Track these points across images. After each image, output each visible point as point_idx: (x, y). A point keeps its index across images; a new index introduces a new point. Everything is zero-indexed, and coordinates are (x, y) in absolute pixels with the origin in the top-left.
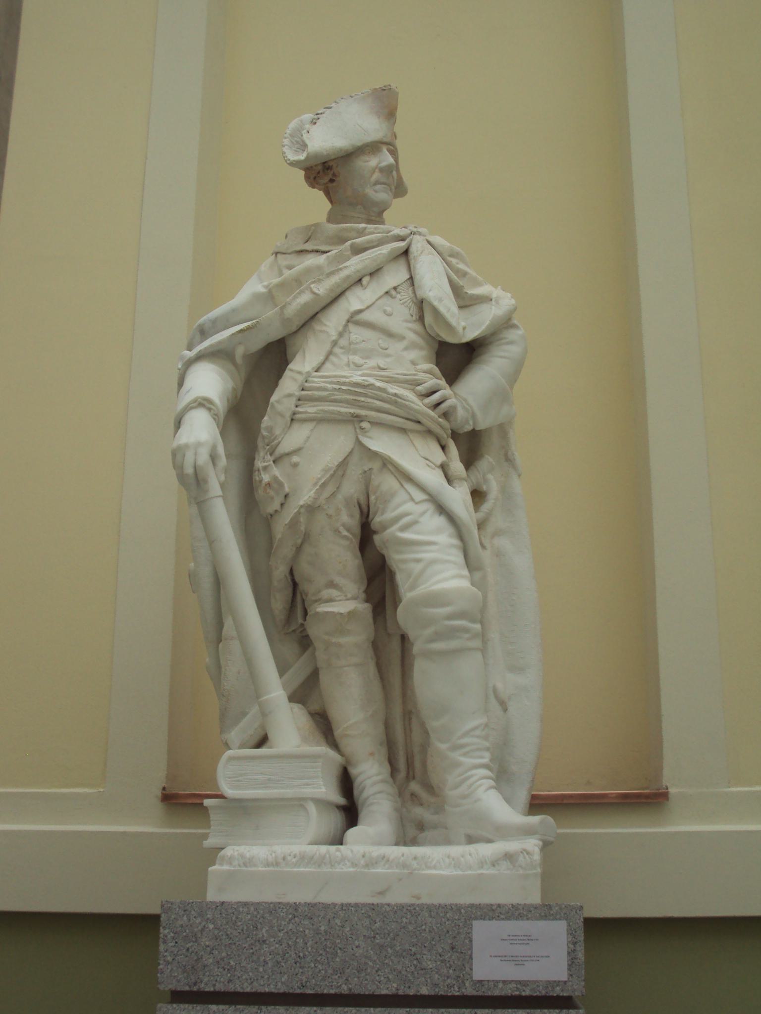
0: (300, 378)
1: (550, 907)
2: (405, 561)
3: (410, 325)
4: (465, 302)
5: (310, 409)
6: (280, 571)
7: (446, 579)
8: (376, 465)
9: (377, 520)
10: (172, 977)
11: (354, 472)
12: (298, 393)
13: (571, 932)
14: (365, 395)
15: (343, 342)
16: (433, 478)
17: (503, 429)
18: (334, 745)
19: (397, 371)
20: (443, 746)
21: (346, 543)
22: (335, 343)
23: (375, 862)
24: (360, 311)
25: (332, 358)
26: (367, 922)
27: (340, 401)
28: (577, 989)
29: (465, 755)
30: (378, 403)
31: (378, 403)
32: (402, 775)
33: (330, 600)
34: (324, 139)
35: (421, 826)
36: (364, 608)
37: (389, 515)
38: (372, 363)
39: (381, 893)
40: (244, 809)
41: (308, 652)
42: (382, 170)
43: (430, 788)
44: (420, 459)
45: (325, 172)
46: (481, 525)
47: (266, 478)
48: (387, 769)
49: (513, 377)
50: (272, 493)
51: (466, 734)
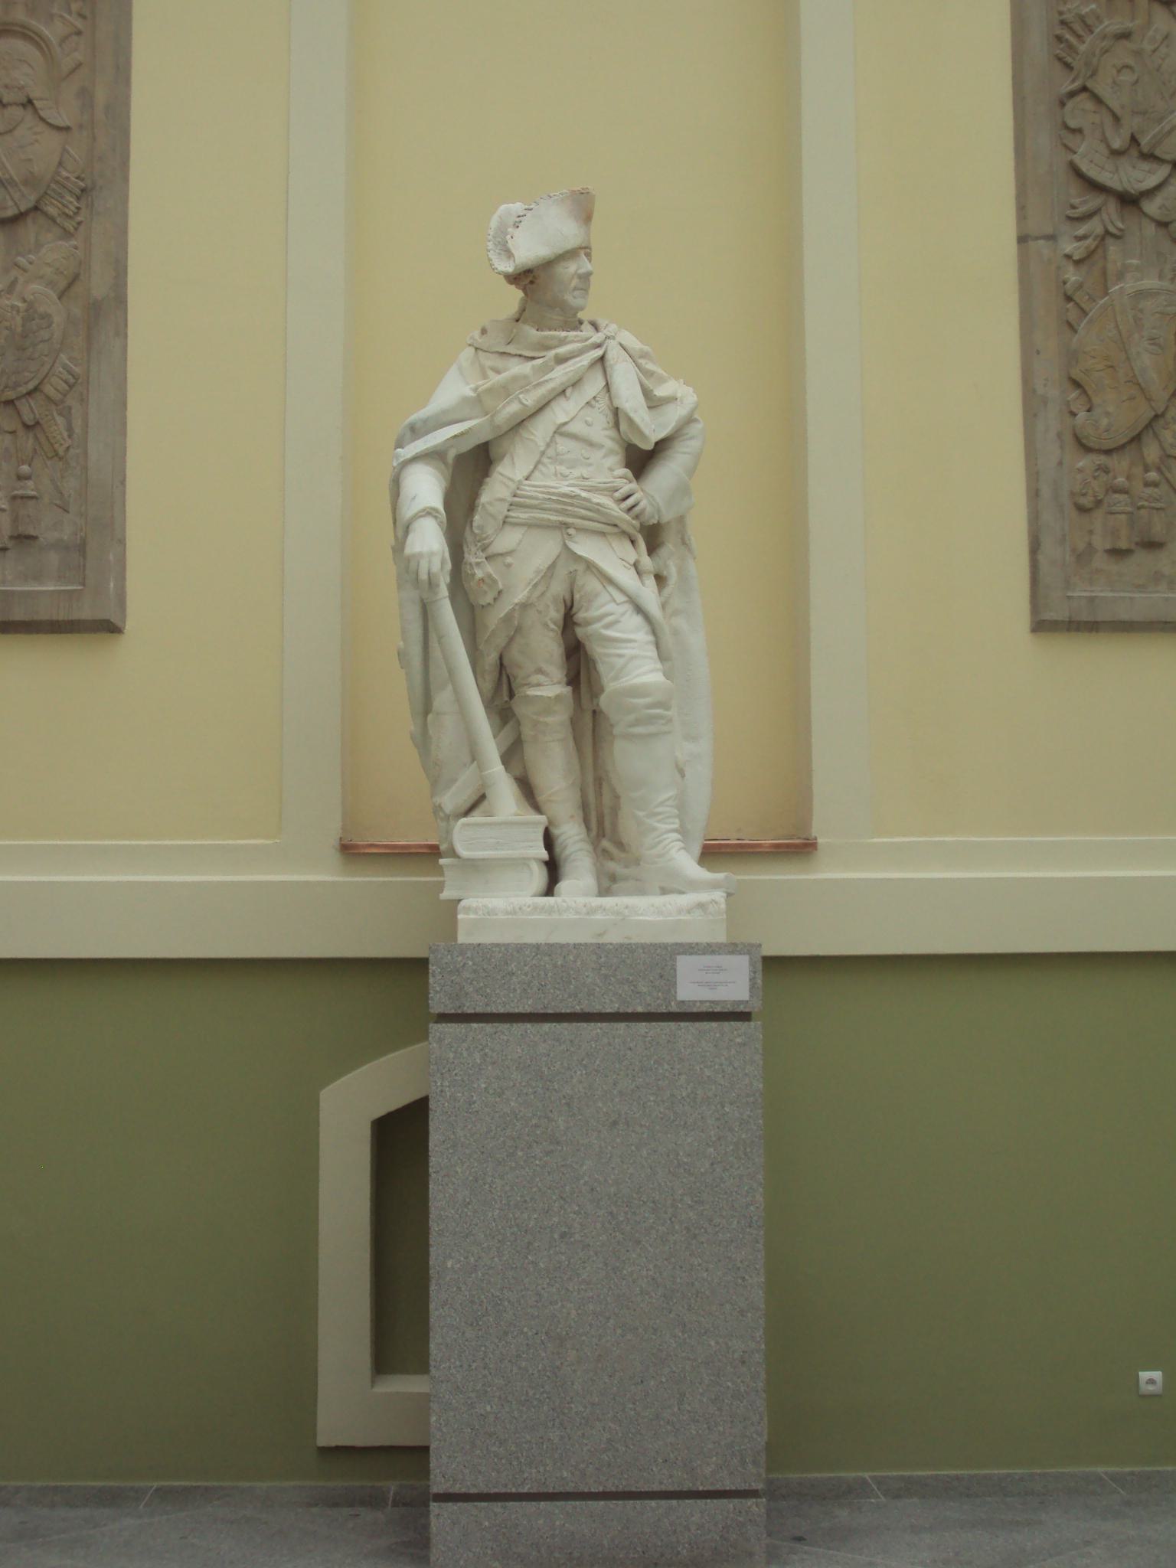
0: (513, 486)
1: (735, 945)
2: (609, 655)
3: (607, 433)
4: (654, 403)
5: (522, 515)
6: (491, 658)
7: (645, 674)
8: (581, 568)
9: (581, 616)
10: (439, 1003)
11: (562, 572)
12: (510, 499)
13: (752, 964)
14: (572, 505)
15: (551, 452)
16: (626, 577)
17: (681, 520)
18: (537, 808)
19: (601, 479)
20: (641, 814)
21: (551, 634)
22: (543, 453)
23: (583, 912)
24: (565, 424)
25: (540, 466)
26: (594, 958)
27: (550, 510)
28: (756, 1006)
29: (659, 821)
30: (583, 512)
31: (583, 512)
32: (594, 833)
33: (539, 685)
34: (528, 249)
35: (613, 878)
36: (566, 690)
37: (594, 613)
38: (576, 473)
39: (600, 935)
40: (475, 867)
41: (511, 723)
42: (580, 277)
43: (620, 845)
44: (615, 559)
45: (526, 278)
46: (664, 606)
47: (479, 574)
48: (584, 830)
49: (691, 472)
50: (485, 588)
51: (662, 804)
